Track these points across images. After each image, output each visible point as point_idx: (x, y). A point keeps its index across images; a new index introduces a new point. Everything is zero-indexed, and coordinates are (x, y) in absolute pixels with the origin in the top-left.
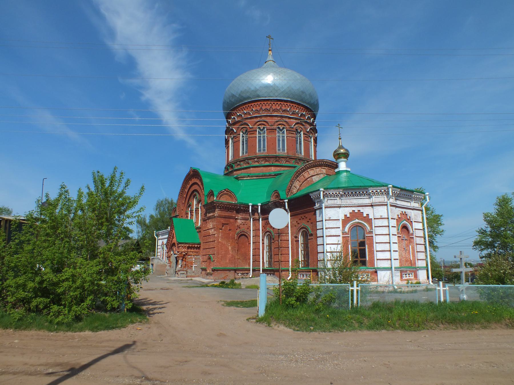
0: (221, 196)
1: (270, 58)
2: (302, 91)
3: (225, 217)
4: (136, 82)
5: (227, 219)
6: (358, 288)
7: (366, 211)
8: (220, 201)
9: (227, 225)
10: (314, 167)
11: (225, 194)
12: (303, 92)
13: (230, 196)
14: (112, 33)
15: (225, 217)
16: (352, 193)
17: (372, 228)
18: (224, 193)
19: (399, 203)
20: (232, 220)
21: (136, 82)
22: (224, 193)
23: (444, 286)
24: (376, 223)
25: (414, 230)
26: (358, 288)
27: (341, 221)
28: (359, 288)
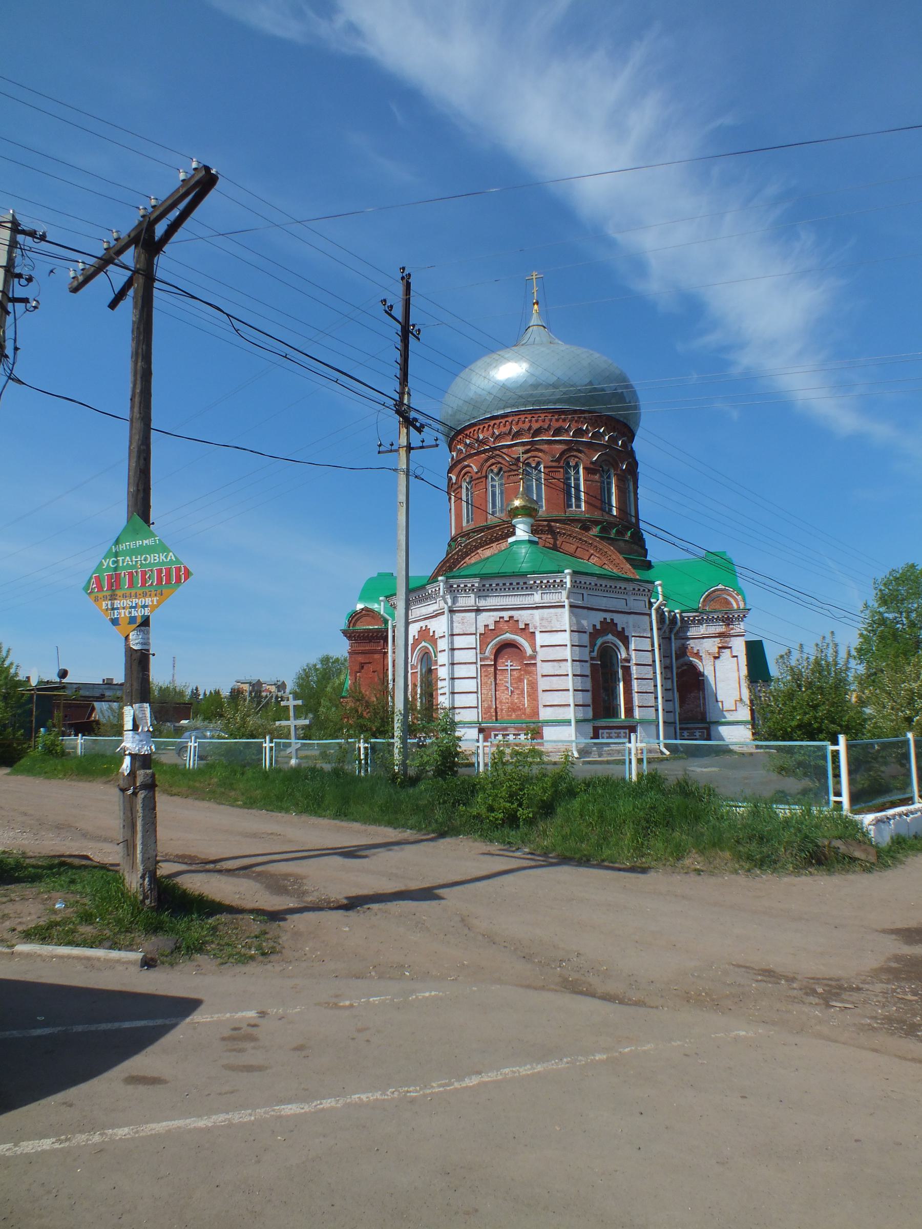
0: (357, 620)
1: (535, 320)
2: (531, 385)
3: (363, 653)
4: (712, 339)
5: (368, 655)
6: (271, 745)
7: (523, 617)
8: (357, 628)
9: (370, 665)
10: (493, 542)
11: (365, 615)
12: (535, 386)
13: (373, 617)
14: (639, 266)
15: (363, 653)
16: (511, 584)
17: (534, 651)
18: (362, 614)
19: (482, 603)
20: (376, 656)
21: (712, 339)
22: (362, 614)
23: (271, 742)
24: (540, 639)
25: (538, 648)
26: (271, 745)
27: (588, 633)
28: (196, 744)
